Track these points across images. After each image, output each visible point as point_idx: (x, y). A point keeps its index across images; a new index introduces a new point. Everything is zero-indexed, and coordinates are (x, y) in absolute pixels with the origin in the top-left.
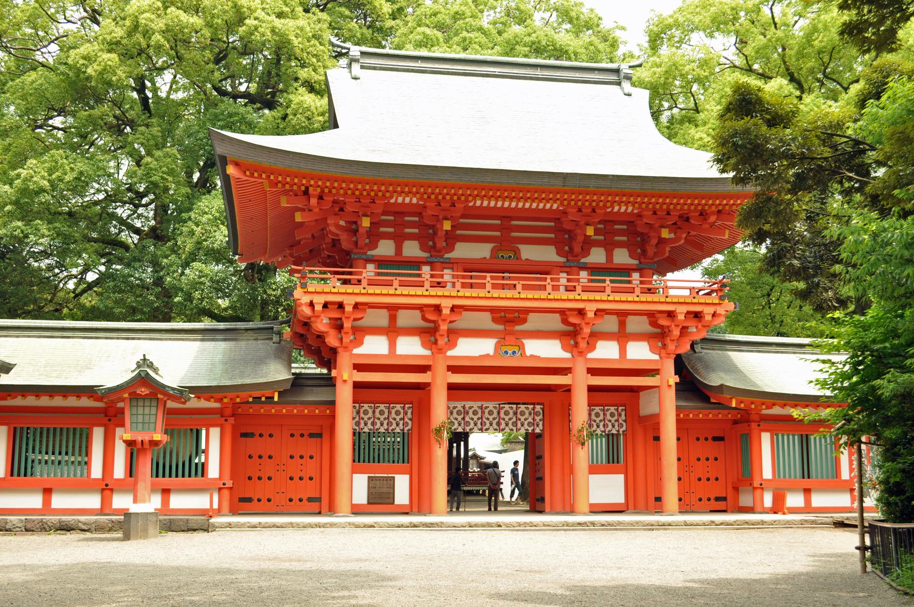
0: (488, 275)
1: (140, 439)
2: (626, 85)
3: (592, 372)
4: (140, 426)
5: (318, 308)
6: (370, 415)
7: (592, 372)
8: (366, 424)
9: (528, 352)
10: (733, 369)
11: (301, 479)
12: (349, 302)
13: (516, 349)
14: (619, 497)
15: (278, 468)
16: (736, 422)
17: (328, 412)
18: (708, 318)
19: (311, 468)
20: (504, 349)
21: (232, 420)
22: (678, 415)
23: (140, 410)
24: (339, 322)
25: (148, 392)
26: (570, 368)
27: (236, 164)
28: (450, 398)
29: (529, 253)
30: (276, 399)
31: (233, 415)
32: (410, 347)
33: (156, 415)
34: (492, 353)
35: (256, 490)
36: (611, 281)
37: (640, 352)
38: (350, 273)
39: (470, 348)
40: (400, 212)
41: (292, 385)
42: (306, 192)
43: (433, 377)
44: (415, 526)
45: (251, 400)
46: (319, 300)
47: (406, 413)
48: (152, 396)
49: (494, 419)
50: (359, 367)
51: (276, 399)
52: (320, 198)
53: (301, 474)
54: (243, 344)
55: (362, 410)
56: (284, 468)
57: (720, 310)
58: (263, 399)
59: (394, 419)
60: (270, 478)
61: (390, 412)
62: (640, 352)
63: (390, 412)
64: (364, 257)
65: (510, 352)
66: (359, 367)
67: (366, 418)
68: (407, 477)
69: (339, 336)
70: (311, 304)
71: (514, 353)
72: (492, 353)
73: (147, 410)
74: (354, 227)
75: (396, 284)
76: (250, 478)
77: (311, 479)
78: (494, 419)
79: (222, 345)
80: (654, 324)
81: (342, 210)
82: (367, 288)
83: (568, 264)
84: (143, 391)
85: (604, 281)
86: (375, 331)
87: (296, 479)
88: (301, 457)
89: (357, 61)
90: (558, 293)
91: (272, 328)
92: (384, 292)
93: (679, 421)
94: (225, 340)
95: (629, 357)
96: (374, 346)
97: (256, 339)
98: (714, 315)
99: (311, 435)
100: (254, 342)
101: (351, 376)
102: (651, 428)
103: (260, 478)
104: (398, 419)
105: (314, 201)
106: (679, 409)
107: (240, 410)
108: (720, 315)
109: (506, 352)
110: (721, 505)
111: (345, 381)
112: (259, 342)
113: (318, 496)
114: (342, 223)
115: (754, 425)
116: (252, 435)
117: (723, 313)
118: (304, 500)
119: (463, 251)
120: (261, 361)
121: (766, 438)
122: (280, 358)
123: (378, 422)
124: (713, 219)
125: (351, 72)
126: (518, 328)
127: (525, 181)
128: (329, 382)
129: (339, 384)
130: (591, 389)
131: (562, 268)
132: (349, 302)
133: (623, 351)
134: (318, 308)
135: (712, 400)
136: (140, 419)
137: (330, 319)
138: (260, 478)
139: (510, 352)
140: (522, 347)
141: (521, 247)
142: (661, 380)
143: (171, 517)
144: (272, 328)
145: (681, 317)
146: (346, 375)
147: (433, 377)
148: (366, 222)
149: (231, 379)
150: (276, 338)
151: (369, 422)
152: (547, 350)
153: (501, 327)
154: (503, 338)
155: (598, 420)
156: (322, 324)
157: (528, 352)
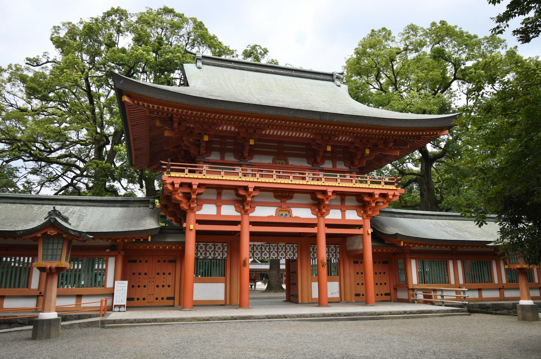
0: (338, 174)
1: (48, 266)
2: (338, 82)
3: (328, 226)
4: (50, 257)
5: (177, 186)
6: (204, 249)
7: (328, 226)
8: (201, 254)
9: (294, 215)
10: (396, 226)
11: (163, 286)
12: (251, 186)
13: (287, 213)
14: (221, 296)
15: (150, 280)
16: (394, 254)
17: (180, 248)
18: (391, 197)
19: (169, 280)
20: (281, 213)
21: (123, 253)
22: (373, 250)
23: (50, 246)
24: (188, 196)
25: (56, 233)
26: (316, 224)
27: (129, 96)
28: (251, 240)
29: (293, 162)
30: (149, 240)
31: (124, 250)
32: (229, 211)
33: (62, 249)
34: (274, 215)
35: (135, 303)
36: (340, 176)
37: (352, 216)
38: (195, 167)
39: (265, 212)
40: (224, 136)
41: (160, 233)
42: (171, 119)
43: (241, 228)
44: (235, 319)
45: (134, 240)
46: (177, 182)
47: (223, 248)
48: (59, 236)
49: (203, 251)
50: (199, 222)
51: (149, 240)
52: (180, 124)
53: (163, 284)
54: (131, 209)
55: (199, 247)
56: (154, 280)
57: (397, 193)
58: (142, 240)
59: (219, 252)
60: (145, 286)
61: (215, 248)
62: (352, 216)
63: (215, 248)
64: (203, 160)
65: (284, 214)
66: (199, 222)
67: (201, 251)
68: (223, 285)
69: (188, 204)
70: (173, 184)
71: (286, 215)
72: (274, 215)
73: (55, 246)
74: (198, 143)
75: (223, 173)
76: (134, 274)
77: (169, 286)
78: (203, 251)
79: (120, 209)
80: (238, 195)
81: (191, 132)
82: (205, 175)
83: (350, 170)
84: (52, 232)
85: (336, 176)
86: (335, 207)
87: (160, 286)
88: (164, 274)
89: (199, 59)
90: (310, 182)
91: (149, 200)
92: (216, 178)
93: (373, 253)
94: (121, 207)
95: (347, 218)
96: (208, 210)
97: (140, 207)
98: (394, 195)
99: (170, 261)
100: (138, 208)
101: (194, 227)
102: (358, 258)
103: (139, 286)
104: (219, 252)
105: (176, 125)
106: (373, 247)
107: (128, 247)
108: (397, 195)
109: (282, 215)
110: (388, 298)
111: (191, 230)
112: (141, 208)
113: (173, 296)
114: (191, 140)
115: (408, 256)
116: (135, 261)
117: (398, 194)
118: (165, 299)
119: (256, 160)
120: (141, 218)
121: (413, 263)
122: (153, 217)
123: (217, 253)
124: (391, 144)
125: (197, 65)
126: (288, 201)
127: (299, 116)
128: (182, 231)
129: (187, 231)
130: (328, 236)
131: (310, 169)
132: (195, 183)
133: (219, 211)
134: (177, 186)
135: (386, 242)
136: (50, 252)
137: (184, 193)
138: (139, 286)
139: (284, 214)
140: (290, 212)
141: (288, 158)
142: (364, 231)
143: (80, 313)
144: (149, 200)
145: (377, 196)
146: (192, 226)
147: (241, 228)
148: (206, 138)
149: (122, 228)
150: (151, 206)
151: (203, 253)
152: (303, 214)
153: (279, 201)
154: (280, 208)
155: (210, 251)
156: (179, 196)
157: (294, 215)
